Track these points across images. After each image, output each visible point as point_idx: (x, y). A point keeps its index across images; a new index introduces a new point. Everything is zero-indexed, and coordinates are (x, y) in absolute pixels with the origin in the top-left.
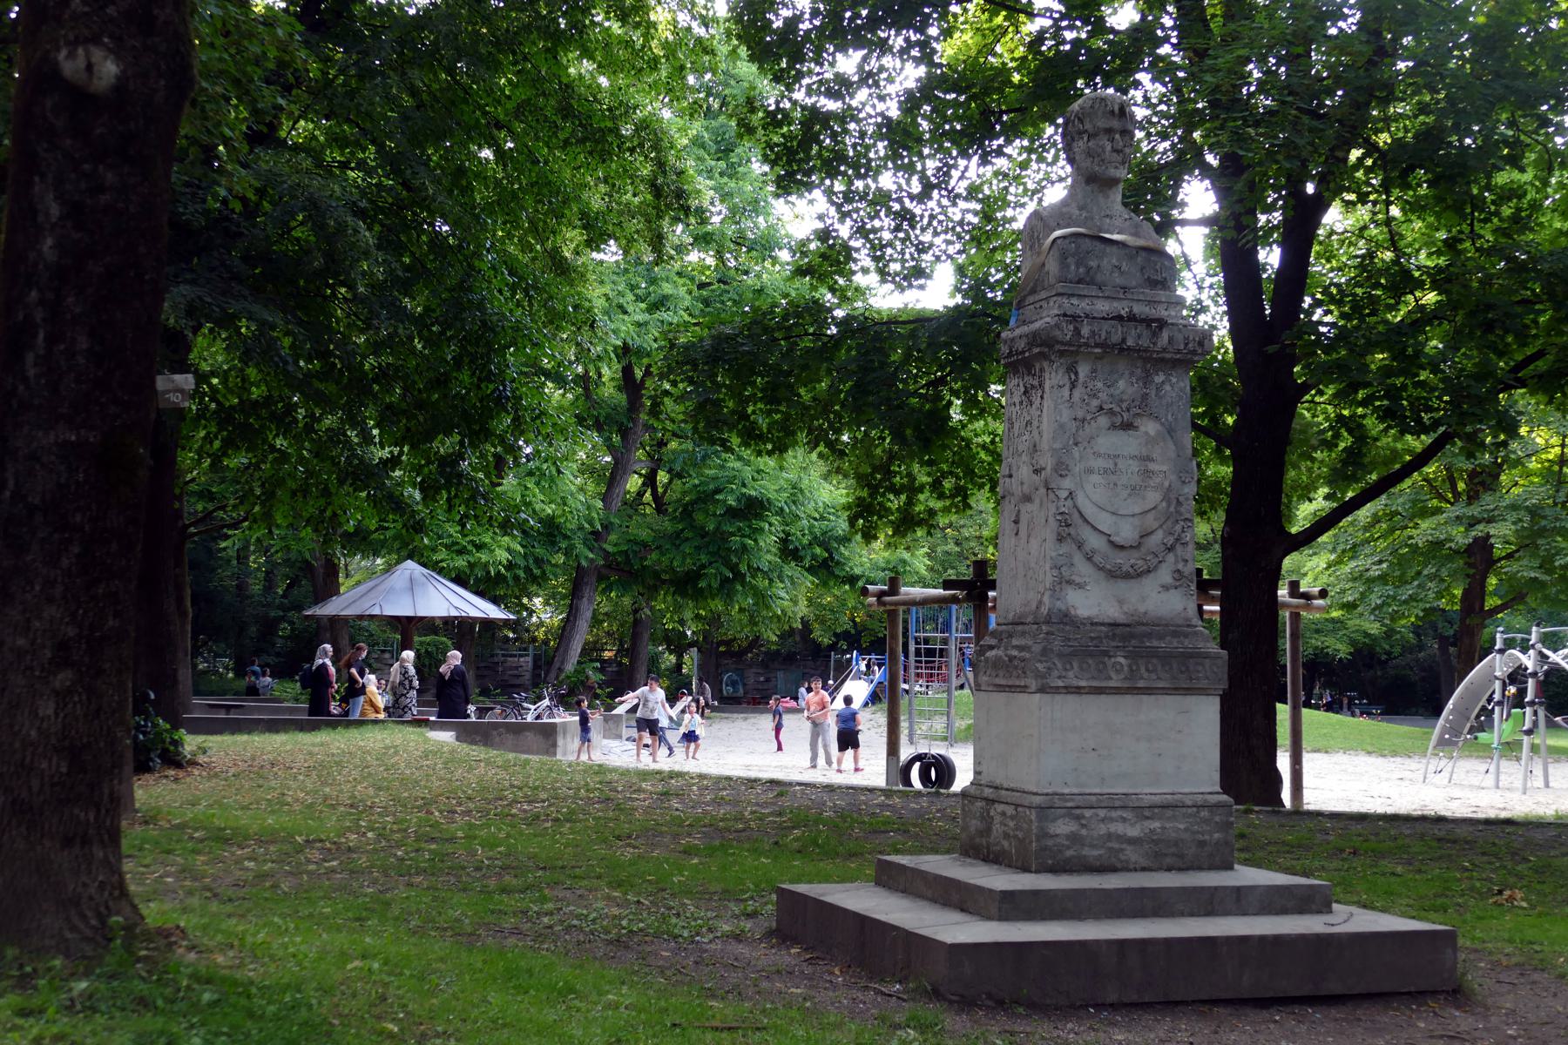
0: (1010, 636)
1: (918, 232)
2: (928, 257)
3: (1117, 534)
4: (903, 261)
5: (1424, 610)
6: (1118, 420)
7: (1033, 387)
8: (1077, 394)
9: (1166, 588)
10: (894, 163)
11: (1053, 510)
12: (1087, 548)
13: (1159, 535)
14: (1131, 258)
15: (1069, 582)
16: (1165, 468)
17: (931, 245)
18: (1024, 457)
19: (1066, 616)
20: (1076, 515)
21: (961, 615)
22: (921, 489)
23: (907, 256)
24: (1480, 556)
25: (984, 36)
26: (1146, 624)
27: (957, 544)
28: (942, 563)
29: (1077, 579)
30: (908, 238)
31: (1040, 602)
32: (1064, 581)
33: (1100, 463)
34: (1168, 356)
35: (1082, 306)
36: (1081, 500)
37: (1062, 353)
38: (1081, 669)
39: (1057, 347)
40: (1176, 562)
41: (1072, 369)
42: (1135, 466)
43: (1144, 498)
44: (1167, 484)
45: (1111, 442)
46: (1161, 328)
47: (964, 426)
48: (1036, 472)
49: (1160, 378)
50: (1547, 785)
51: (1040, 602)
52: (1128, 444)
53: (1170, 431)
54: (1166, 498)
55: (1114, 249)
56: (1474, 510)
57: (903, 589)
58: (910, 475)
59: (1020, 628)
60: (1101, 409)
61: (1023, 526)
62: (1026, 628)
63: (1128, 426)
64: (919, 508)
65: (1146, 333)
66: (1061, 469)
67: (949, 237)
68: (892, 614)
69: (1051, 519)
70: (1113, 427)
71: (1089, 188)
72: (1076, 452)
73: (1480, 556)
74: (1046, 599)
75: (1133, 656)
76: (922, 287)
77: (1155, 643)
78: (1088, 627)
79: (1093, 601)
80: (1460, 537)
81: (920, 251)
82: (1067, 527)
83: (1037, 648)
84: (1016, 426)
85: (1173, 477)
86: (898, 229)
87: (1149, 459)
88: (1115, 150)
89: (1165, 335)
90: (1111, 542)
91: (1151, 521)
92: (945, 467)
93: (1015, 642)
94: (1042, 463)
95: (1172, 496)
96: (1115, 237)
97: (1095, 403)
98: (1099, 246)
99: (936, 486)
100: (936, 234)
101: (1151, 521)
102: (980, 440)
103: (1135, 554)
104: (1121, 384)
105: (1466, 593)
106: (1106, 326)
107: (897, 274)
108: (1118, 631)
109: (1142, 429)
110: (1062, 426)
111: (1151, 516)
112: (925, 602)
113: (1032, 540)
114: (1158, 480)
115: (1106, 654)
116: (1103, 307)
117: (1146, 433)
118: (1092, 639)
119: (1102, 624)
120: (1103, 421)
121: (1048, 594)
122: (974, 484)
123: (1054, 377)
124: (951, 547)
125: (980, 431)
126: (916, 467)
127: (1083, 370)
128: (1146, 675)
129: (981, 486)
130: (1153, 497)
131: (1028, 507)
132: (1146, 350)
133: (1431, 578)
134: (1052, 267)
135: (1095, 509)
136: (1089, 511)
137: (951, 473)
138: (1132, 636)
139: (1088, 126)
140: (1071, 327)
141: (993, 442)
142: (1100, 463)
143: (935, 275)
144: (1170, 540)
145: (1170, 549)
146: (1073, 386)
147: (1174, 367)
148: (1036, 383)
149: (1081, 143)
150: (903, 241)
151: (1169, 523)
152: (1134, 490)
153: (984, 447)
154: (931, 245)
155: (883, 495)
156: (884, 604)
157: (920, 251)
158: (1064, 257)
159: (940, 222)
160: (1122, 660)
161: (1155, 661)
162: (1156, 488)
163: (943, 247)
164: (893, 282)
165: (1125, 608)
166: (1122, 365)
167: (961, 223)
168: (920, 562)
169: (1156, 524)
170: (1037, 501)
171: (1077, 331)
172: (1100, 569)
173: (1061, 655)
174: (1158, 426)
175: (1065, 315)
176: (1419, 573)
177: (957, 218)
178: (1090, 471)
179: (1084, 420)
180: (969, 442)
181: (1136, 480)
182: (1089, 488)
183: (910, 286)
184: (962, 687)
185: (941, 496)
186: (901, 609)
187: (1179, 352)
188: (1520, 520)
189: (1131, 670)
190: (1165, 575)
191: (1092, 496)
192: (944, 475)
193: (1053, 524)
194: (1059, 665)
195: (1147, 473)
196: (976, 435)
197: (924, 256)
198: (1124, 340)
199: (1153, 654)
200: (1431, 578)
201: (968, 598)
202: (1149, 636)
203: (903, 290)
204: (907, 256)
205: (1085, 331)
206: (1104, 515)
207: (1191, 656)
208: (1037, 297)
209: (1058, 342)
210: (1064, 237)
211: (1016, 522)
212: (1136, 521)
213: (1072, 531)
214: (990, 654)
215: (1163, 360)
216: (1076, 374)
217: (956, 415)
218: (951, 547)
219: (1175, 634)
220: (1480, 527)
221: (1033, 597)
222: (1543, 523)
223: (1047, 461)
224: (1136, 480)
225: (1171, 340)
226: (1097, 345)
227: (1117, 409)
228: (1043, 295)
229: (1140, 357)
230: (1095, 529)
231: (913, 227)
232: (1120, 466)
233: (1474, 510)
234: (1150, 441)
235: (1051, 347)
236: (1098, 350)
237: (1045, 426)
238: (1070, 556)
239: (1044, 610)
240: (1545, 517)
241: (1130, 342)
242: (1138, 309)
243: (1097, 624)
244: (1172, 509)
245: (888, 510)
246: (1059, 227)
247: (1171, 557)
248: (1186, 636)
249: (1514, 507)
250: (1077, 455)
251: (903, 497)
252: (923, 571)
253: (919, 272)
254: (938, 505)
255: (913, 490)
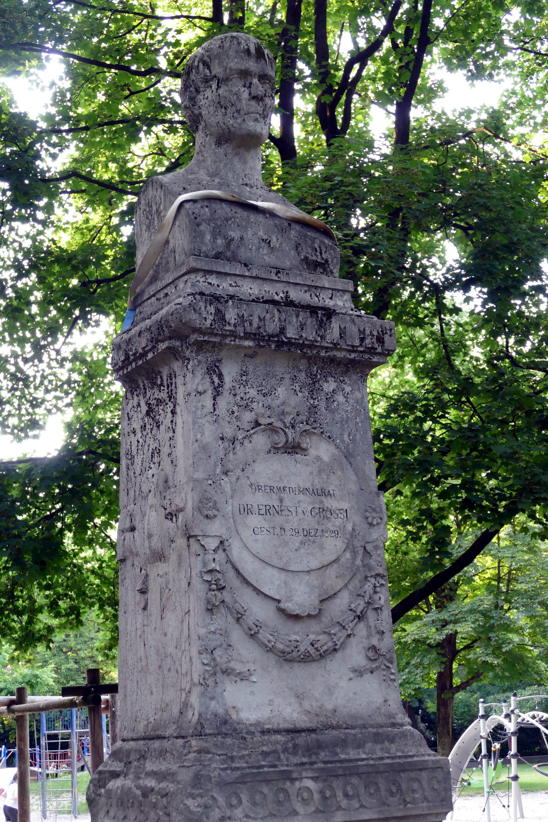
0: (143, 757)
1: (32, 390)
2: (40, 411)
3: (290, 599)
4: (20, 416)
5: (415, 690)
6: (281, 440)
7: (159, 402)
8: (223, 402)
9: (359, 672)
10: (11, 335)
11: (198, 566)
12: (249, 620)
13: (343, 600)
14: (282, 231)
15: (227, 672)
16: (345, 505)
17: (43, 401)
18: (151, 500)
19: (225, 722)
20: (231, 573)
21: (79, 715)
22: (40, 610)
23: (23, 412)
24: (448, 648)
25: (82, 234)
26: (337, 727)
27: (76, 663)
28: (66, 677)
29: (239, 667)
30: (23, 396)
31: (186, 705)
32: (220, 671)
33: (260, 499)
34: (340, 355)
35: (225, 286)
36: (237, 552)
37: (200, 346)
38: (254, 804)
39: (194, 337)
40: (369, 636)
41: (214, 370)
42: (306, 503)
43: (322, 547)
44: (349, 527)
45: (271, 469)
46: (329, 318)
47: (76, 555)
48: (170, 516)
49: (329, 386)
50: (522, 817)
51: (186, 705)
52: (295, 473)
53: (348, 456)
54: (349, 547)
55: (260, 218)
56: (444, 615)
57: (30, 698)
58: (30, 598)
59: (156, 744)
60: (257, 424)
61: (153, 596)
62: (166, 744)
63: (293, 449)
64: (39, 626)
65: (311, 322)
66: (207, 509)
67: (58, 394)
68: (20, 720)
69: (196, 582)
70: (275, 449)
71: (221, 151)
72: (226, 484)
73: (448, 648)
74: (194, 699)
75: (325, 776)
76: (36, 437)
77: (352, 754)
78: (258, 738)
79: (261, 699)
80: (435, 636)
81: (33, 406)
82: (219, 589)
83: (185, 776)
84: (138, 460)
85: (357, 519)
86: (13, 389)
87: (325, 493)
88: (255, 98)
89: (335, 325)
90: (282, 611)
91: (333, 580)
92: (60, 590)
93: (150, 766)
94: (178, 502)
95: (358, 544)
96: (260, 204)
97: (248, 417)
98: (240, 213)
99: (53, 606)
100: (47, 391)
101: (333, 580)
102: (89, 566)
103: (314, 626)
104: (281, 392)
105: (440, 674)
106: (259, 310)
107: (15, 427)
108: (301, 739)
109: (312, 452)
110: (204, 448)
111: (332, 572)
112: (48, 707)
113: (169, 615)
114: (338, 522)
115: (287, 776)
116: (250, 289)
117: (318, 458)
118: (265, 754)
119: (278, 732)
120: (261, 441)
121: (196, 691)
122: (86, 604)
123: (189, 380)
124: (72, 665)
125: (89, 557)
126: (36, 591)
127: (230, 371)
128: (344, 803)
129: (92, 605)
130: (333, 546)
131: (161, 568)
132: (311, 346)
133: (417, 667)
134: (180, 240)
135: (257, 564)
136: (249, 566)
137: (66, 595)
138: (320, 746)
139: (217, 70)
140: (212, 309)
141: (100, 567)
142: (260, 499)
143: (47, 427)
144: (359, 604)
145: (360, 617)
146: (217, 393)
147: (346, 372)
148: (164, 395)
149: (208, 93)
150: (21, 398)
151: (356, 582)
152: (308, 536)
153: (93, 572)
154: (43, 401)
155: (8, 616)
156: (13, 711)
157: (33, 406)
158: (195, 222)
159: (50, 382)
160: (309, 784)
161: (355, 780)
162: (336, 533)
163: (54, 402)
164: (12, 433)
165: (306, 705)
166: (281, 367)
167: (69, 382)
168: (48, 675)
169: (340, 584)
170: (173, 558)
171: (220, 316)
172: (270, 650)
173: (222, 784)
174: (332, 449)
175: (202, 294)
176: (408, 663)
177: (64, 378)
178: (247, 510)
179: (233, 441)
180: (80, 568)
181: (310, 522)
182: (246, 534)
183: (27, 436)
184: (82, 769)
185: (58, 615)
186: (27, 714)
187: (353, 349)
188: (477, 620)
189: (324, 798)
190: (355, 655)
191: (252, 545)
192: (59, 597)
193: (199, 586)
194: (221, 800)
195: (324, 513)
196: (86, 562)
197: (37, 410)
198: (282, 330)
199: (350, 770)
200: (417, 667)
201: (85, 702)
202: (343, 743)
203: (20, 439)
204: (23, 412)
205: (231, 315)
206: (270, 571)
207: (402, 769)
208: (160, 284)
209: (195, 330)
210: (194, 201)
211: (143, 592)
212: (313, 579)
213: (226, 596)
214: (114, 784)
215: (332, 360)
216: (220, 376)
217: (68, 539)
218: (72, 665)
219: (378, 738)
220: (450, 626)
221: (173, 697)
222: (492, 621)
223: (186, 498)
224: (310, 522)
225: (343, 333)
226: (247, 336)
227: (279, 424)
228: (169, 278)
229: (304, 355)
230: (259, 592)
231: (27, 386)
232: (287, 503)
233: (444, 615)
234: (324, 469)
235: (183, 338)
236: (247, 343)
237: (180, 450)
238: (225, 634)
239: (192, 716)
240: (493, 618)
241: (291, 333)
242: (296, 295)
243: (269, 731)
244: (358, 562)
245: (12, 629)
246: (185, 190)
247: (361, 629)
248: (392, 740)
249: (472, 611)
250: (228, 488)
251: (25, 618)
252: (51, 682)
253: (34, 424)
254: (55, 622)
255: (33, 611)
